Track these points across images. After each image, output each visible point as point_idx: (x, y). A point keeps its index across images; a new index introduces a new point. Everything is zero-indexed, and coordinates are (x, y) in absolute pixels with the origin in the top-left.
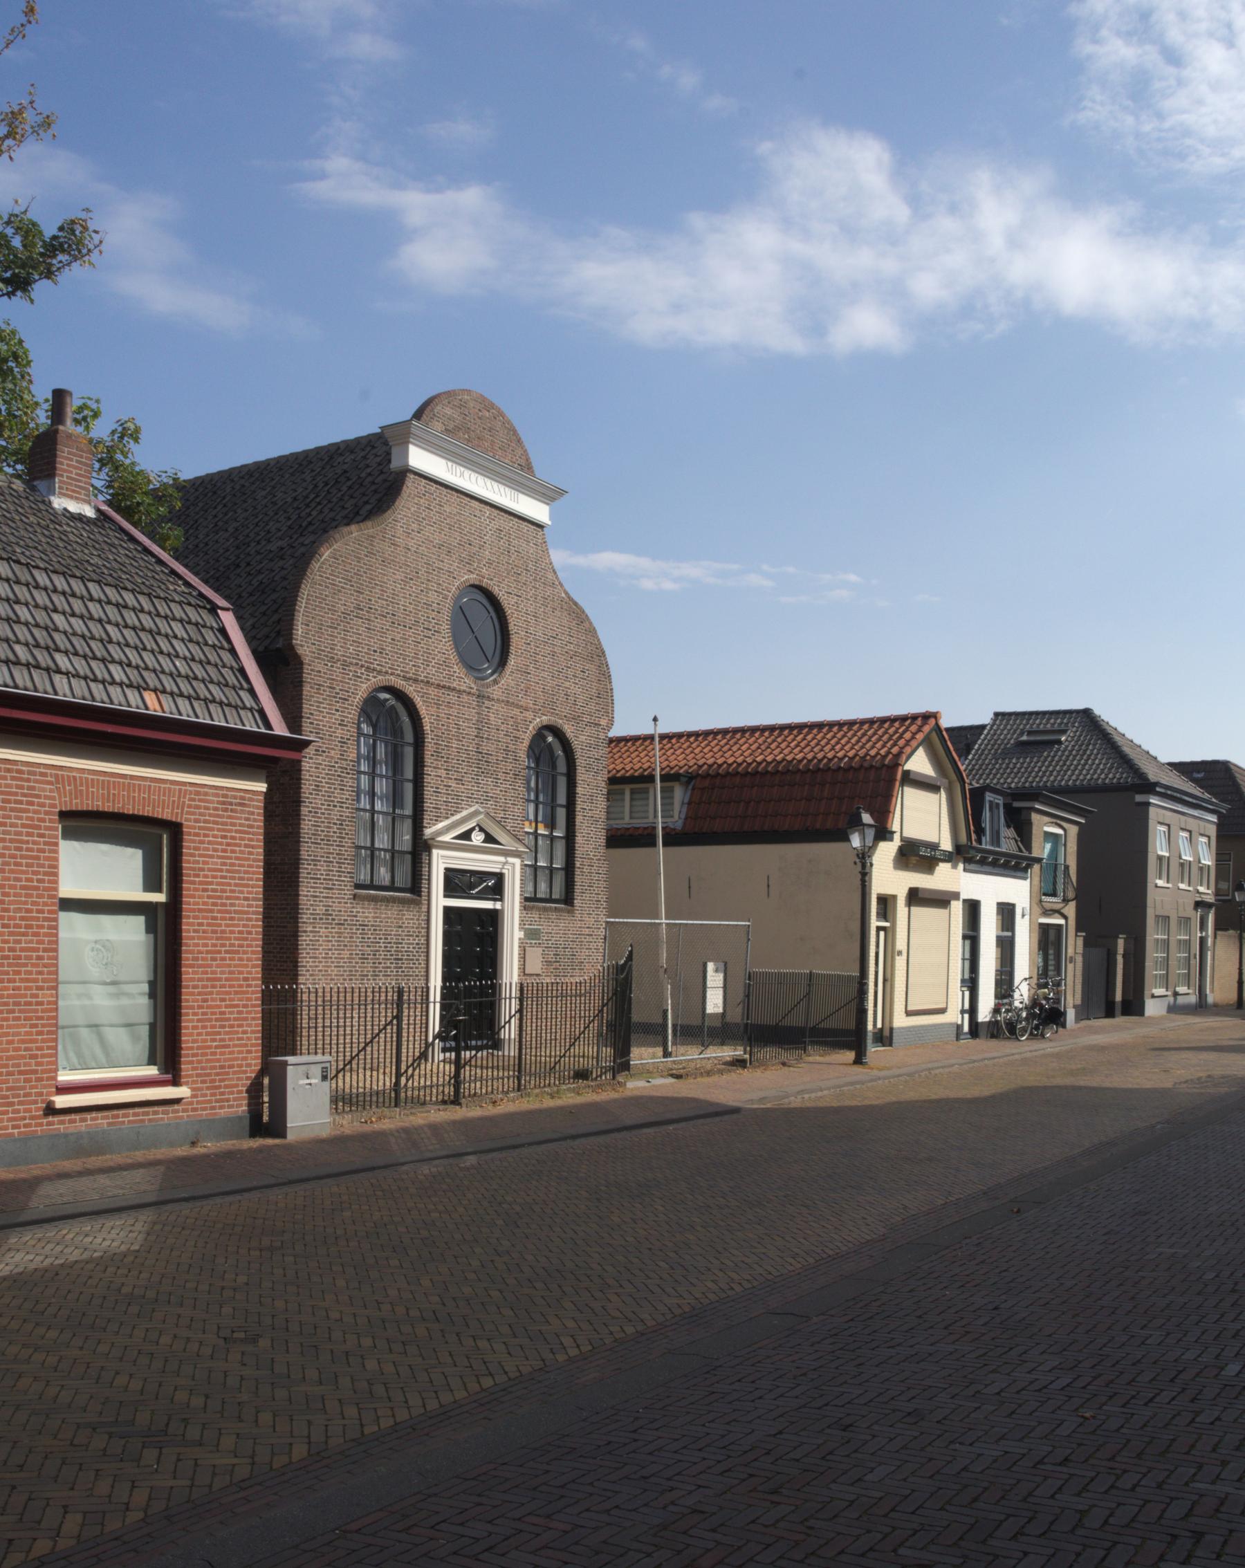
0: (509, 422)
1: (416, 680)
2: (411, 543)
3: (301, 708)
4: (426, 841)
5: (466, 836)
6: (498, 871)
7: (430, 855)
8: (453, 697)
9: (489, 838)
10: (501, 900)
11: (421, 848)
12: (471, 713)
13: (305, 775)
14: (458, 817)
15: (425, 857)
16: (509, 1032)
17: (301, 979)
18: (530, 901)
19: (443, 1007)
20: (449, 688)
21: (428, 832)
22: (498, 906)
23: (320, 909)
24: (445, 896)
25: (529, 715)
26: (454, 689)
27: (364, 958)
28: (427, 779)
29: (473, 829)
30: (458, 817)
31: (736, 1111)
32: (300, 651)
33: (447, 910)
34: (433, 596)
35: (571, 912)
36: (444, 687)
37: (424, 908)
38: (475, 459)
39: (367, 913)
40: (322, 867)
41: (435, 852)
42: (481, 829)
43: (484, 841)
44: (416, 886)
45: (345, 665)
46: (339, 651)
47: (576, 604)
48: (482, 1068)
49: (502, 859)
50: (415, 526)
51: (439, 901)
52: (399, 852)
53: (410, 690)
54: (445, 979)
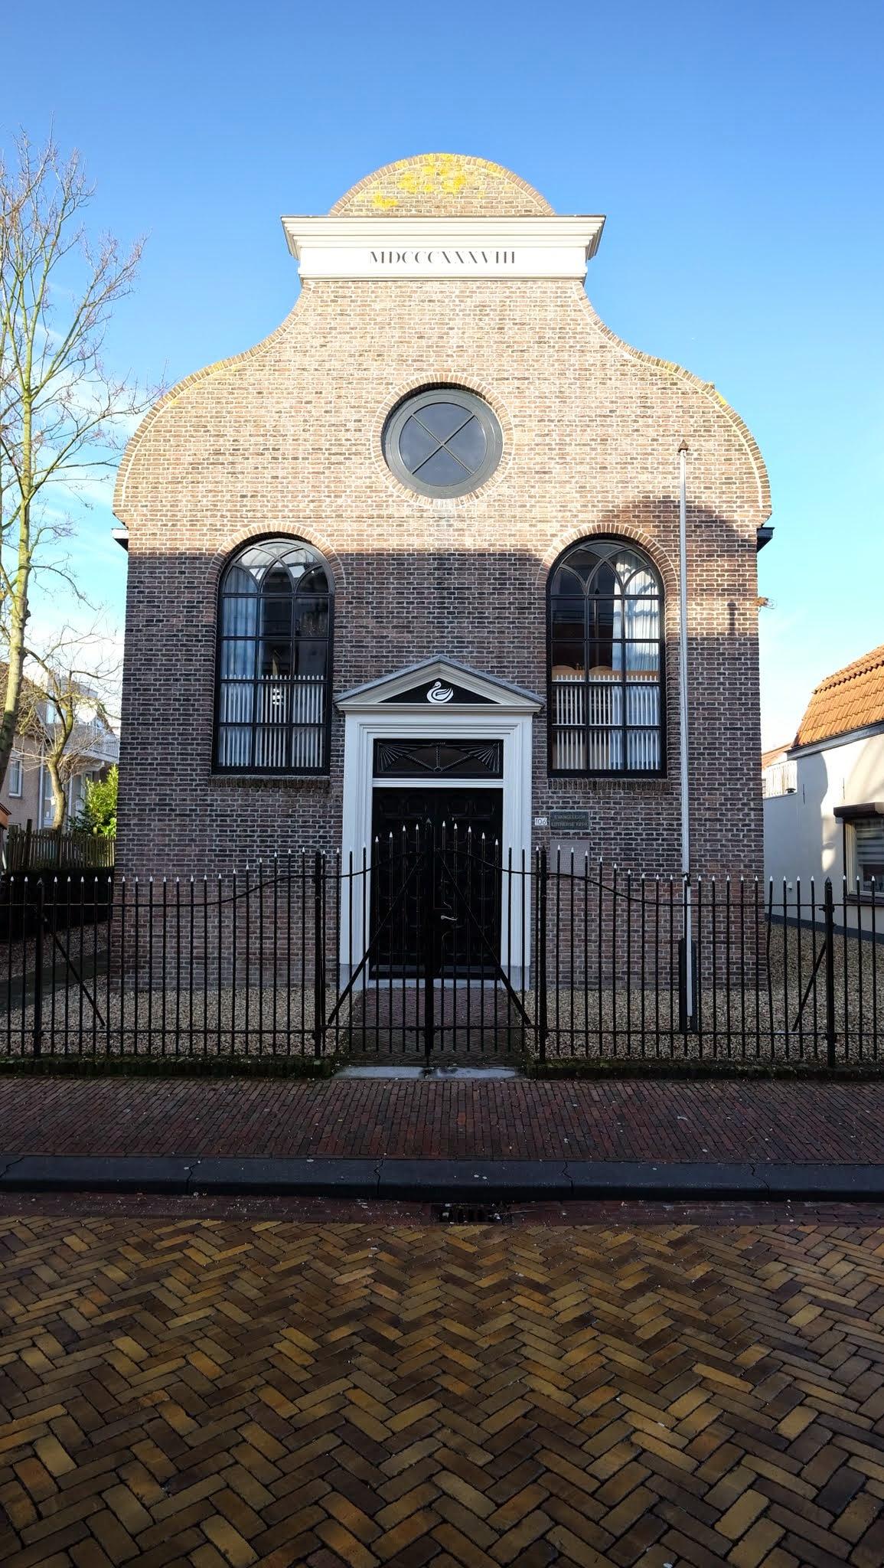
5: (418, 695)
9: (462, 696)
23: (152, 798)
29: (431, 685)
39: (231, 800)
42: (446, 685)
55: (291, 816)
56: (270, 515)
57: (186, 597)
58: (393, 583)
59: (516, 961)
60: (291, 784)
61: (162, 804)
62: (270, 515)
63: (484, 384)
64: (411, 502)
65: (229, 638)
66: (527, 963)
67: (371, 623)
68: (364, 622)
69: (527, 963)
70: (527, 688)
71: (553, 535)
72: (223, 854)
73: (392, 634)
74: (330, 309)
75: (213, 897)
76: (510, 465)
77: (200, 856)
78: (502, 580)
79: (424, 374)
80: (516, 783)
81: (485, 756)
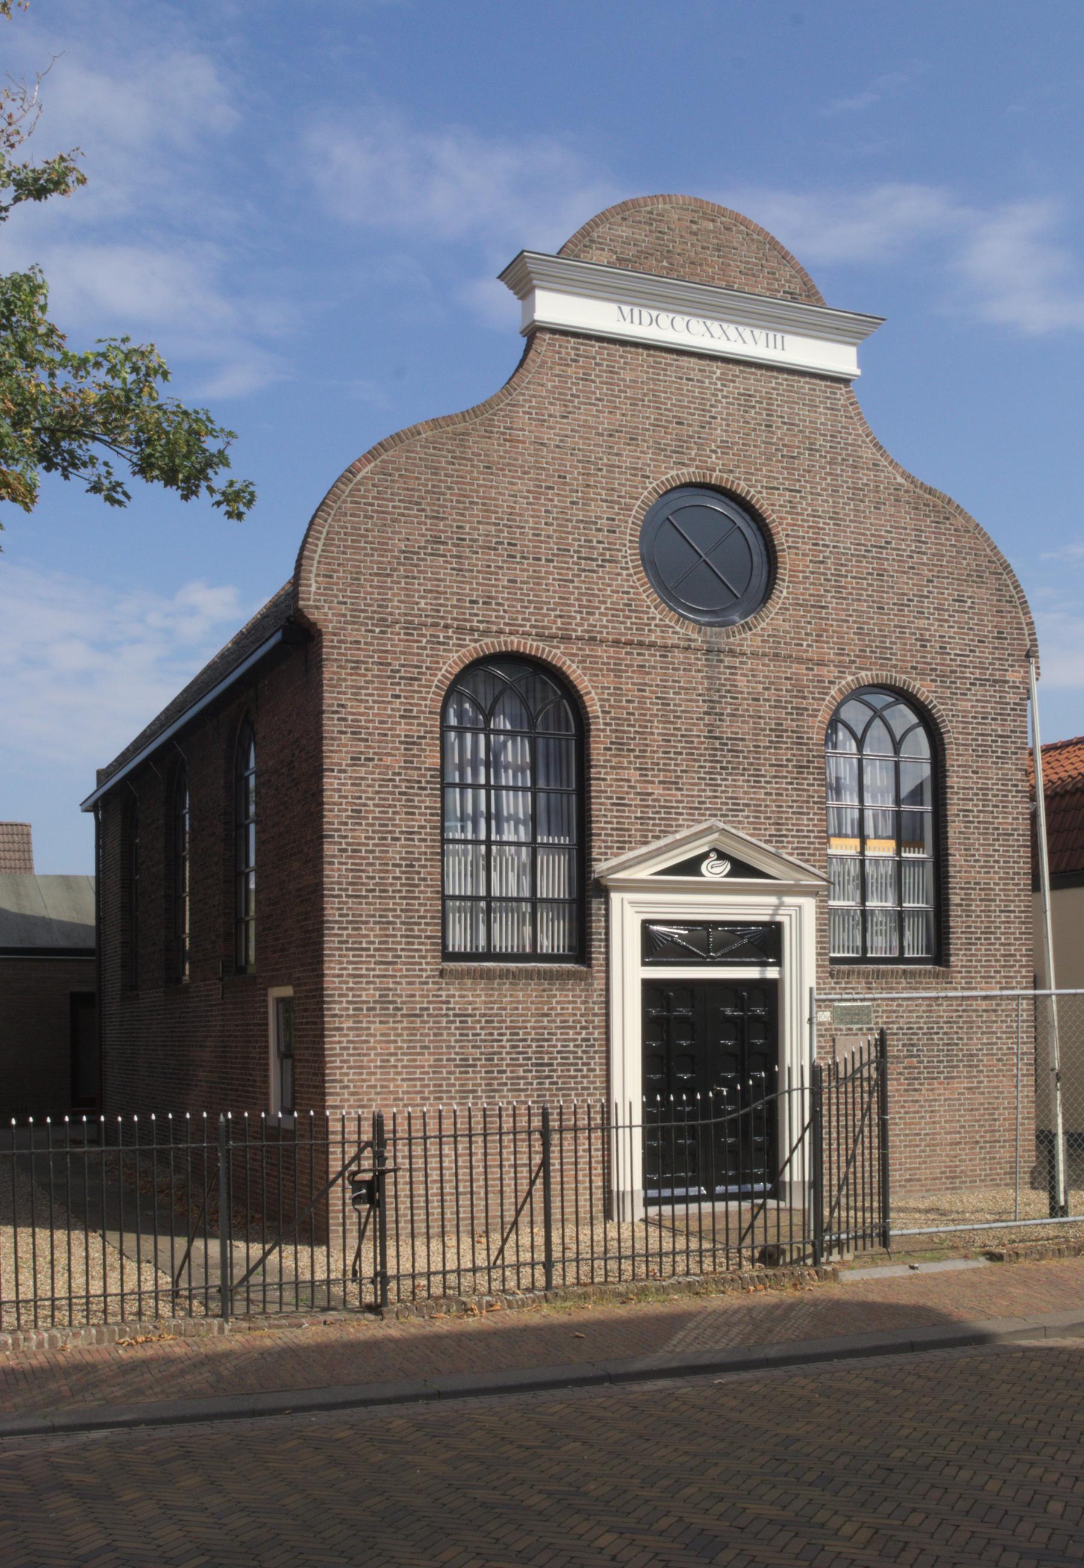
0: (760, 231)
1: (565, 639)
2: (547, 435)
3: (321, 699)
4: (597, 881)
5: (691, 867)
6: (766, 918)
7: (607, 903)
8: (652, 658)
9: (740, 868)
10: (779, 963)
11: (586, 896)
12: (699, 680)
13: (330, 796)
14: (662, 843)
15: (596, 905)
16: (797, 1170)
17: (330, 1101)
18: (835, 967)
19: (648, 1135)
20: (641, 644)
21: (600, 867)
22: (772, 973)
23: (371, 994)
24: (644, 964)
25: (829, 672)
26: (652, 645)
27: (465, 1064)
28: (595, 786)
29: (704, 856)
30: (662, 843)
31: (981, 1339)
32: (314, 616)
33: (649, 986)
34: (597, 509)
35: (945, 975)
36: (629, 643)
37: (599, 984)
38: (671, 292)
39: (473, 997)
40: (372, 933)
41: (615, 897)
42: (722, 856)
43: (730, 875)
44: (583, 947)
45: (409, 628)
46: (396, 608)
47: (931, 491)
48: (864, 1210)
49: (773, 900)
50: (556, 410)
51: (628, 973)
52: (543, 900)
53: (555, 654)
54: (649, 1088)
55: (546, 1015)
56: (507, 629)
57: (402, 729)
58: (658, 728)
59: (797, 1177)
60: (488, 975)
61: (383, 1001)
62: (507, 629)
63: (752, 491)
64: (678, 629)
65: (524, 789)
66: (807, 1179)
67: (634, 775)
68: (625, 774)
69: (807, 1179)
70: (807, 861)
71: (830, 682)
72: (465, 1064)
73: (658, 791)
74: (570, 371)
75: (507, 1125)
76: (785, 594)
77: (437, 1066)
78: (778, 730)
79: (685, 470)
80: (800, 971)
81: (765, 942)
